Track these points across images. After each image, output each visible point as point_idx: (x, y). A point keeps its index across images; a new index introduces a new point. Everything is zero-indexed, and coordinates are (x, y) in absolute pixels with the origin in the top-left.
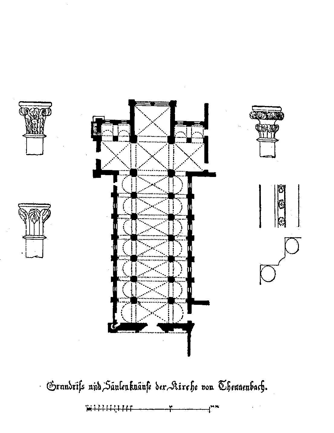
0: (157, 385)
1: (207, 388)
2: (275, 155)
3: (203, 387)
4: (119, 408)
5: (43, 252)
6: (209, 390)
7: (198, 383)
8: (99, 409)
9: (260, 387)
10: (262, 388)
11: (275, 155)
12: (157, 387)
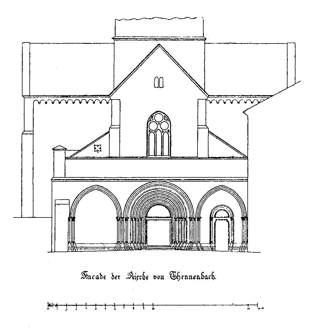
0: (113, 276)
1: (159, 278)
2: (163, 86)
3: (154, 277)
4: (77, 305)
5: (22, 56)
6: (140, 282)
7: (150, 274)
8: (134, 305)
9: (211, 277)
10: (213, 278)
11: (163, 86)
12: (113, 277)
